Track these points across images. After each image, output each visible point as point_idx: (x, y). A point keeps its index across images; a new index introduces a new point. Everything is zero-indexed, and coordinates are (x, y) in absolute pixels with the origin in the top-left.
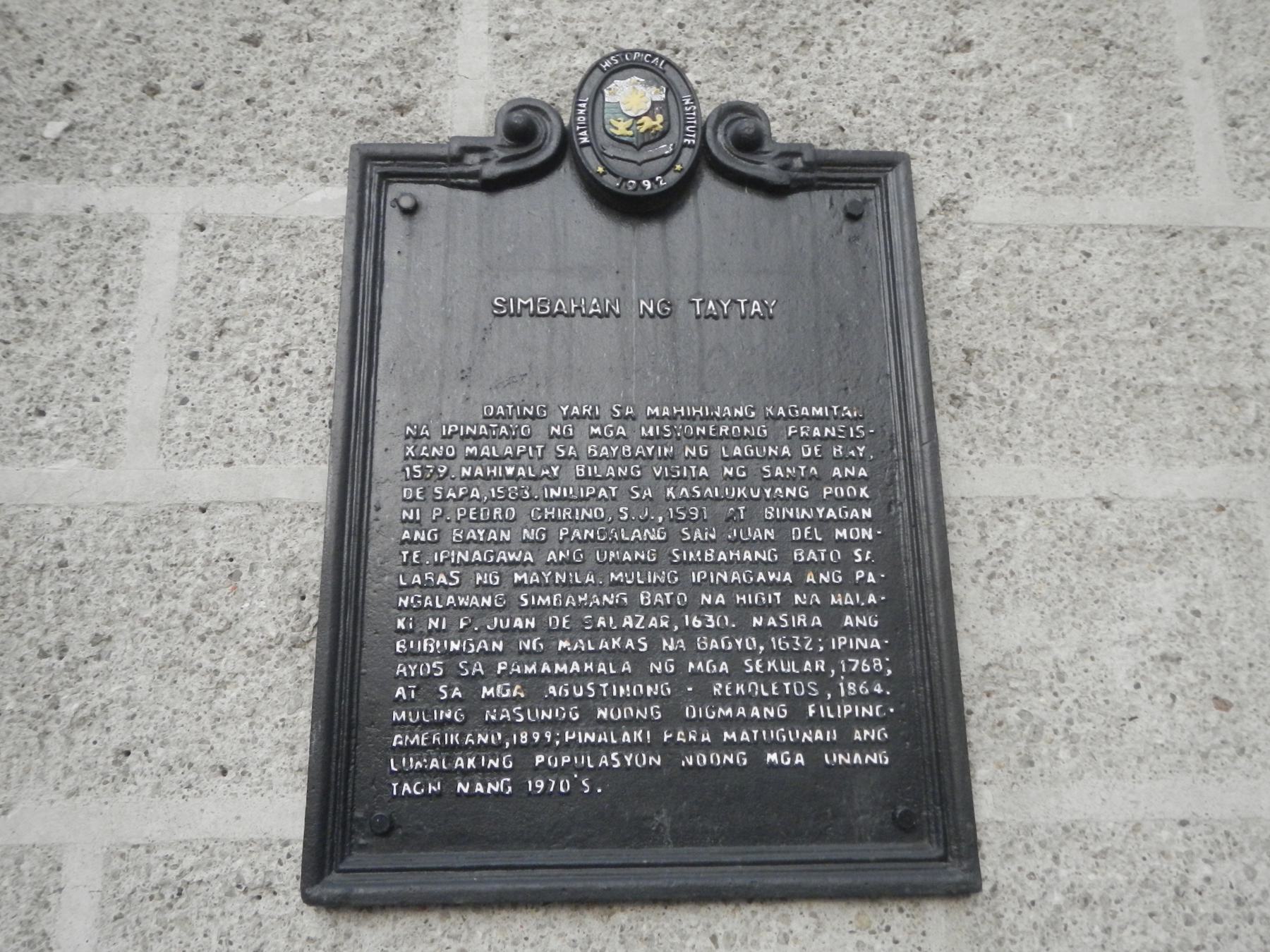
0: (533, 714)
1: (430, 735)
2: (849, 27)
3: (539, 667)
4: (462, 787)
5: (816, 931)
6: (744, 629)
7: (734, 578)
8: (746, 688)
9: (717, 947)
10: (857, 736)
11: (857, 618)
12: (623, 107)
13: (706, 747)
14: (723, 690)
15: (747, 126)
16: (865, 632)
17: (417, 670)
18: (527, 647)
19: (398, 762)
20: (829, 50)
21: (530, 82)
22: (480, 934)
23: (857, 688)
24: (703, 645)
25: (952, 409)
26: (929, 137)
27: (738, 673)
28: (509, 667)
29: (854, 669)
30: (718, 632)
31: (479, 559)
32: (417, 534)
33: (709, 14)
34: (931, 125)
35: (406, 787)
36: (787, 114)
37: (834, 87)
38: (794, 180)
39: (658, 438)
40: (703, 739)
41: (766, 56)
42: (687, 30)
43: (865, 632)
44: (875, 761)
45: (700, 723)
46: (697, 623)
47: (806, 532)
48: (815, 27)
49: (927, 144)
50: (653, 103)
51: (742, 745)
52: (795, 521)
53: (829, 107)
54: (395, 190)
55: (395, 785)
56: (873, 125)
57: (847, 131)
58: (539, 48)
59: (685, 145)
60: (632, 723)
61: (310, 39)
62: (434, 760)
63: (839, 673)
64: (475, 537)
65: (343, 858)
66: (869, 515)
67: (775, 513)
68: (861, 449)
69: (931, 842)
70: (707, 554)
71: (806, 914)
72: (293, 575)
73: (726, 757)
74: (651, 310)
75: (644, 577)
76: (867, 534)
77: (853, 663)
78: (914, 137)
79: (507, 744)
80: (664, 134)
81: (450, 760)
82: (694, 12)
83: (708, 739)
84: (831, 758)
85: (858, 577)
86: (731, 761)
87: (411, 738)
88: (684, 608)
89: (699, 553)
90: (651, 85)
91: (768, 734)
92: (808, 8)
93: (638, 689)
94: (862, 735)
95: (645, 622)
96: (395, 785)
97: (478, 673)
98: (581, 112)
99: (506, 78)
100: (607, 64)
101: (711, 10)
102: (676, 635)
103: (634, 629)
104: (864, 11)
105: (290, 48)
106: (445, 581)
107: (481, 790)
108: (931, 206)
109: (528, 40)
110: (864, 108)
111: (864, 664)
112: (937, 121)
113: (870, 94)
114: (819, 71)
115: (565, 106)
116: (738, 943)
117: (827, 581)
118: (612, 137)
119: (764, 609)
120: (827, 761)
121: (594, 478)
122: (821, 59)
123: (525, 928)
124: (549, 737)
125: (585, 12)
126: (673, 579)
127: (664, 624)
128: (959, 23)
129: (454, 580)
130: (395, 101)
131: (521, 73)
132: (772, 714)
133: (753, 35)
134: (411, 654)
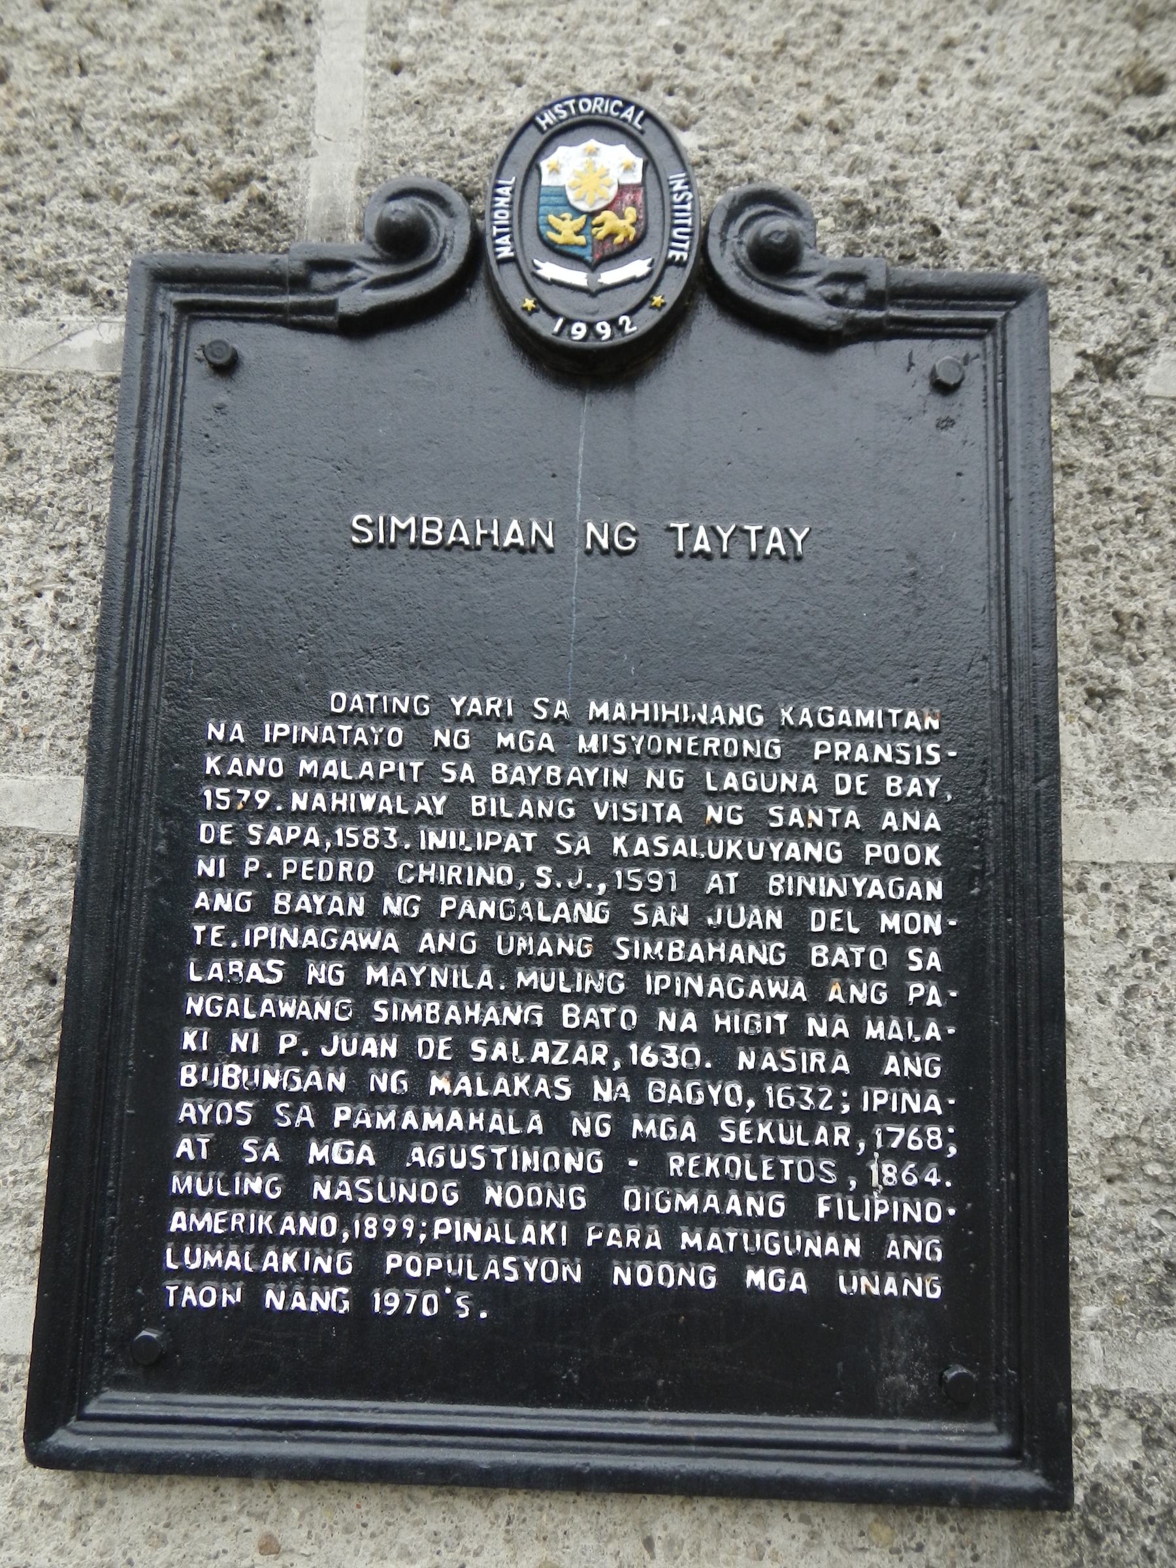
0: (386, 1192)
2: (959, 52)
3: (399, 1119)
5: (807, 1544)
6: (724, 1070)
7: (712, 989)
9: (653, 1557)
10: (892, 1252)
12: (571, 196)
13: (654, 1256)
14: (685, 1168)
15: (777, 225)
17: (212, 1115)
18: (383, 1088)
19: (177, 1257)
20: (924, 92)
22: (296, 1513)
23: (899, 1175)
24: (657, 1095)
25: (1088, 714)
27: (709, 1141)
29: (895, 1145)
30: (682, 1075)
33: (727, 29)
34: (1086, 224)
38: (852, 323)
39: (605, 755)
41: (816, 103)
42: (689, 56)
44: (918, 1293)
45: (645, 1218)
48: (902, 52)
50: (622, 189)
51: (713, 1256)
52: (817, 900)
54: (208, 332)
55: (172, 1289)
57: (945, 234)
58: (445, 88)
59: (670, 262)
61: (83, 72)
63: (871, 1147)
66: (939, 895)
67: (785, 885)
70: (672, 949)
71: (794, 1516)
72: (38, 949)
75: (570, 980)
76: (933, 924)
79: (346, 1236)
81: (257, 1257)
82: (702, 24)
84: (848, 1282)
85: (912, 996)
88: (631, 1035)
92: (892, 17)
93: (551, 1158)
96: (172, 1289)
98: (502, 202)
100: (549, 118)
101: (730, 22)
104: (986, 24)
105: (51, 87)
109: (427, 74)
111: (911, 1137)
112: (1098, 217)
114: (904, 128)
116: (686, 1553)
118: (551, 246)
119: (757, 1042)
121: (500, 820)
122: (909, 107)
123: (364, 1509)
125: (523, 27)
126: (615, 987)
127: (598, 1058)
128: (1144, 43)
133: (798, 64)
134: (204, 1091)
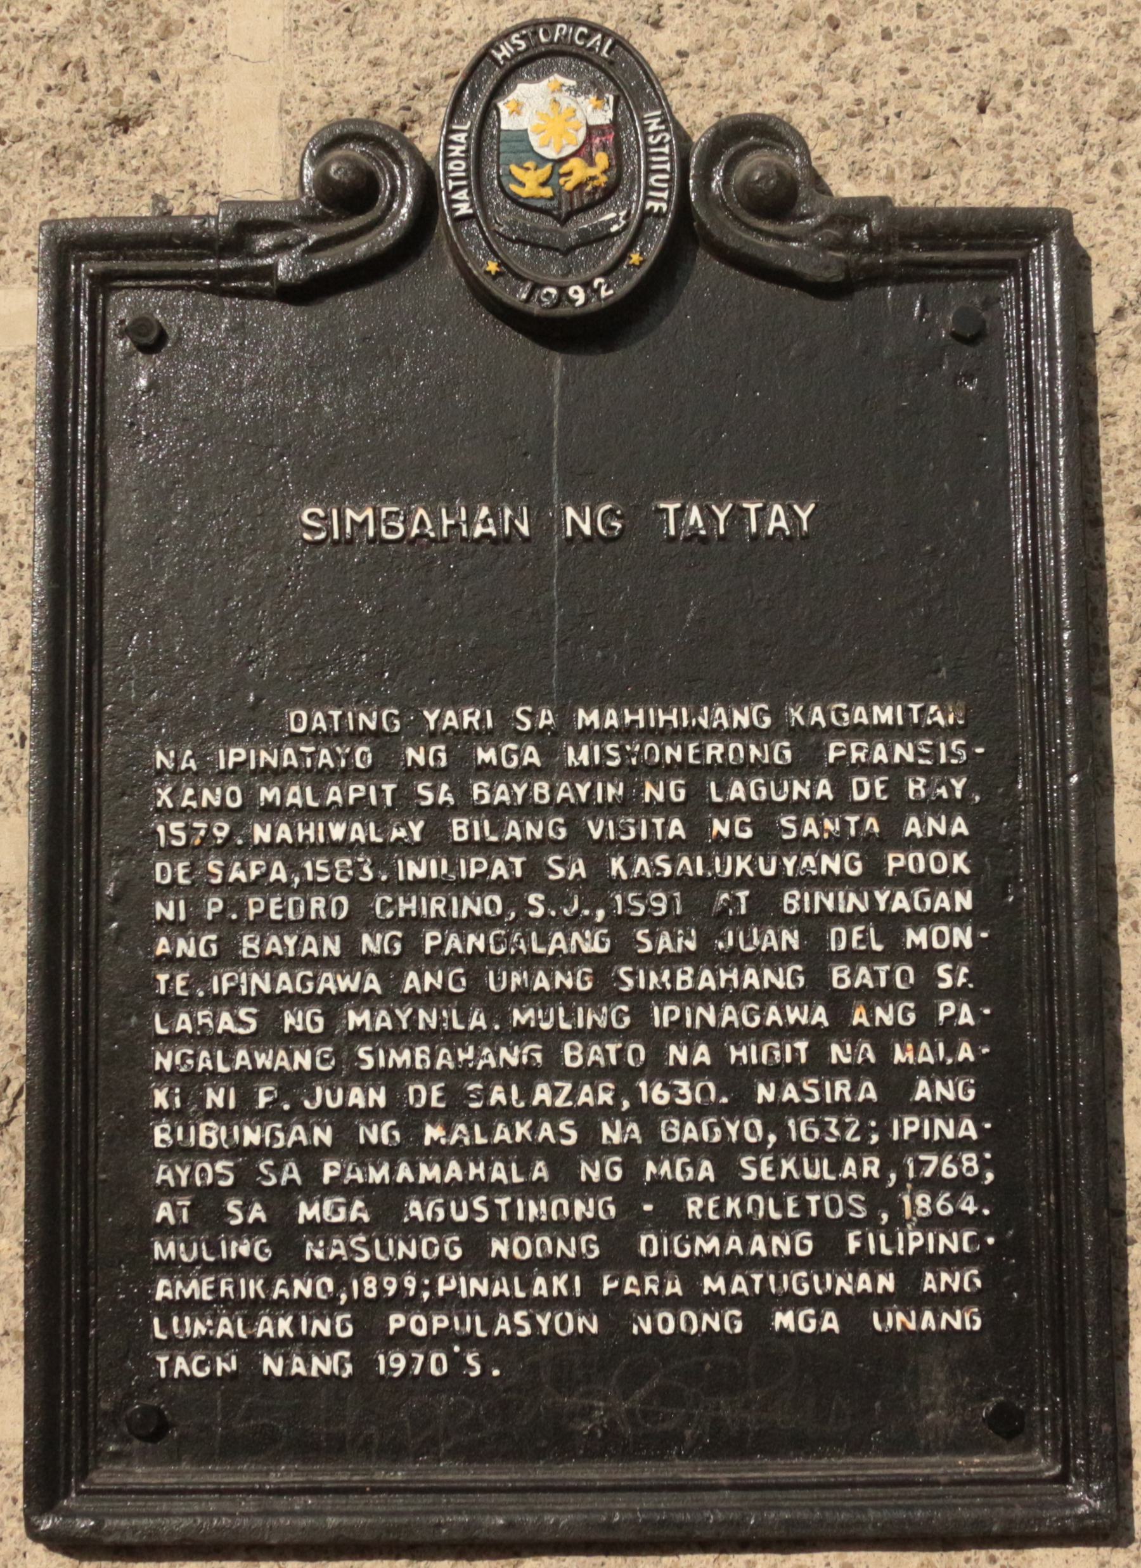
0: (384, 1249)
1: (217, 1283)
3: (393, 1172)
4: (272, 1365)
7: (726, 1019)
8: (742, 1205)
11: (939, 1084)
13: (675, 1304)
14: (704, 1210)
16: (950, 1109)
18: (374, 1140)
19: (166, 1326)
21: (363, 63)
23: (933, 1204)
24: (671, 1134)
26: (1123, 156)
28: (343, 1172)
30: (696, 1113)
31: (289, 988)
32: (181, 944)
35: (180, 1363)
36: (851, 115)
37: (943, 56)
40: (669, 1291)
43: (950, 1109)
44: (957, 1325)
45: (664, 1265)
46: (659, 1096)
47: (856, 937)
49: (1117, 170)
50: (590, 129)
53: (930, 101)
56: (1015, 135)
60: (550, 1265)
62: (224, 1320)
64: (279, 951)
65: (84, 1473)
66: (968, 906)
67: (801, 902)
68: (959, 785)
69: (1044, 1453)
70: (680, 977)
73: (706, 1318)
74: (586, 529)
75: (570, 1016)
76: (963, 937)
77: (929, 1162)
78: (1093, 156)
79: (344, 1297)
80: (610, 191)
81: (250, 1322)
83: (678, 1290)
84: (883, 1319)
85: (942, 1015)
86: (716, 1327)
87: (186, 1285)
89: (666, 975)
90: (587, 93)
91: (779, 1282)
93: (560, 1208)
94: (938, 1280)
95: (573, 1095)
97: (291, 1182)
98: (457, 151)
99: (318, 57)
100: (505, 51)
102: (625, 1117)
103: (553, 1109)
106: (231, 1027)
107: (302, 1371)
108: (1117, 301)
110: (1001, 94)
111: (946, 1165)
113: (1012, 70)
114: (915, 23)
115: (428, 141)
117: (889, 1022)
118: (515, 199)
119: (777, 1073)
120: (878, 1326)
124: (412, 1287)
127: (606, 1098)
129: (246, 1025)
130: (112, 110)
131: (346, 48)
132: (786, 1250)
134: (180, 1152)
